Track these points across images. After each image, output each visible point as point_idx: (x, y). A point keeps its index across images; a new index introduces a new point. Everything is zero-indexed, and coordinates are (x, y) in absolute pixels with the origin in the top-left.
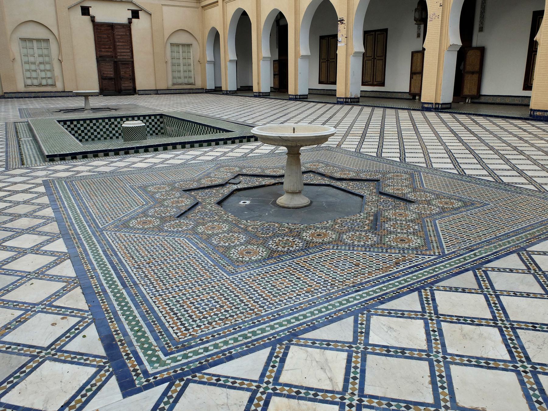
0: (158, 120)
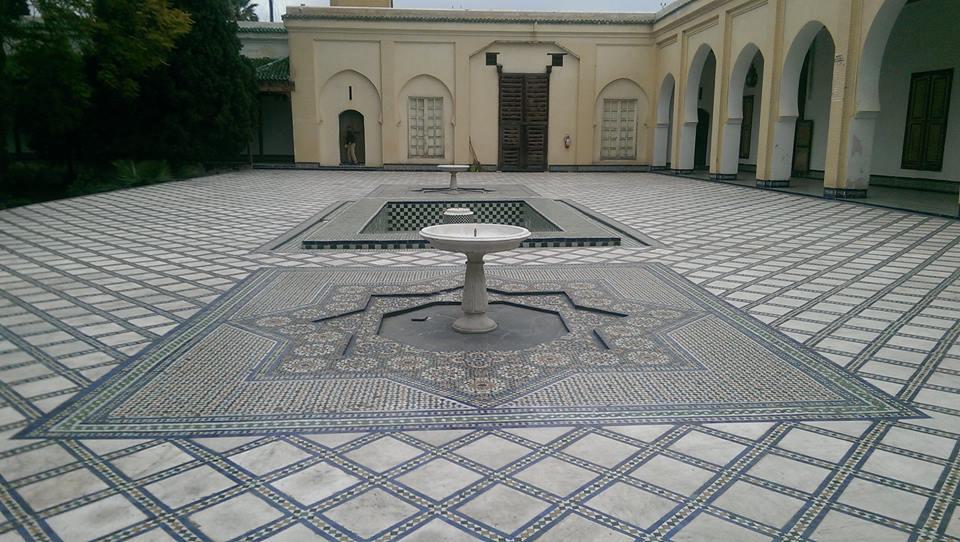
0: (517, 209)
